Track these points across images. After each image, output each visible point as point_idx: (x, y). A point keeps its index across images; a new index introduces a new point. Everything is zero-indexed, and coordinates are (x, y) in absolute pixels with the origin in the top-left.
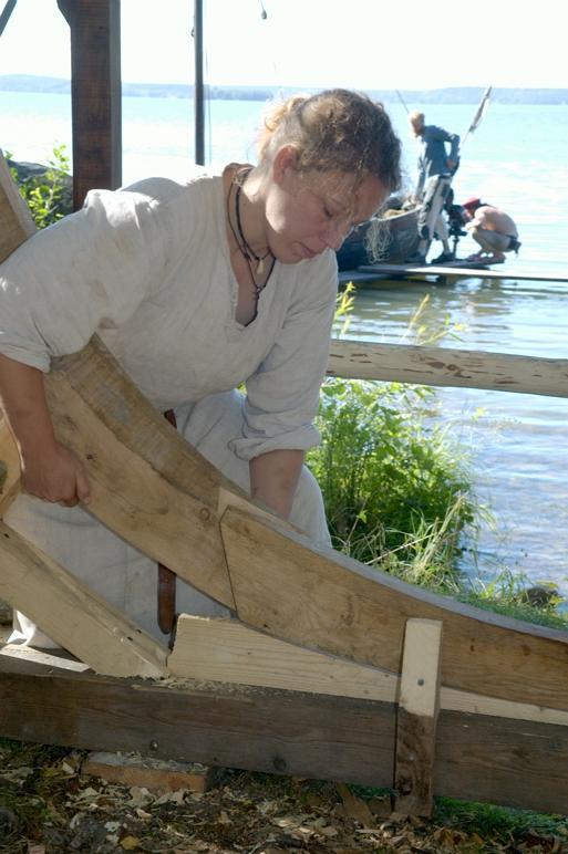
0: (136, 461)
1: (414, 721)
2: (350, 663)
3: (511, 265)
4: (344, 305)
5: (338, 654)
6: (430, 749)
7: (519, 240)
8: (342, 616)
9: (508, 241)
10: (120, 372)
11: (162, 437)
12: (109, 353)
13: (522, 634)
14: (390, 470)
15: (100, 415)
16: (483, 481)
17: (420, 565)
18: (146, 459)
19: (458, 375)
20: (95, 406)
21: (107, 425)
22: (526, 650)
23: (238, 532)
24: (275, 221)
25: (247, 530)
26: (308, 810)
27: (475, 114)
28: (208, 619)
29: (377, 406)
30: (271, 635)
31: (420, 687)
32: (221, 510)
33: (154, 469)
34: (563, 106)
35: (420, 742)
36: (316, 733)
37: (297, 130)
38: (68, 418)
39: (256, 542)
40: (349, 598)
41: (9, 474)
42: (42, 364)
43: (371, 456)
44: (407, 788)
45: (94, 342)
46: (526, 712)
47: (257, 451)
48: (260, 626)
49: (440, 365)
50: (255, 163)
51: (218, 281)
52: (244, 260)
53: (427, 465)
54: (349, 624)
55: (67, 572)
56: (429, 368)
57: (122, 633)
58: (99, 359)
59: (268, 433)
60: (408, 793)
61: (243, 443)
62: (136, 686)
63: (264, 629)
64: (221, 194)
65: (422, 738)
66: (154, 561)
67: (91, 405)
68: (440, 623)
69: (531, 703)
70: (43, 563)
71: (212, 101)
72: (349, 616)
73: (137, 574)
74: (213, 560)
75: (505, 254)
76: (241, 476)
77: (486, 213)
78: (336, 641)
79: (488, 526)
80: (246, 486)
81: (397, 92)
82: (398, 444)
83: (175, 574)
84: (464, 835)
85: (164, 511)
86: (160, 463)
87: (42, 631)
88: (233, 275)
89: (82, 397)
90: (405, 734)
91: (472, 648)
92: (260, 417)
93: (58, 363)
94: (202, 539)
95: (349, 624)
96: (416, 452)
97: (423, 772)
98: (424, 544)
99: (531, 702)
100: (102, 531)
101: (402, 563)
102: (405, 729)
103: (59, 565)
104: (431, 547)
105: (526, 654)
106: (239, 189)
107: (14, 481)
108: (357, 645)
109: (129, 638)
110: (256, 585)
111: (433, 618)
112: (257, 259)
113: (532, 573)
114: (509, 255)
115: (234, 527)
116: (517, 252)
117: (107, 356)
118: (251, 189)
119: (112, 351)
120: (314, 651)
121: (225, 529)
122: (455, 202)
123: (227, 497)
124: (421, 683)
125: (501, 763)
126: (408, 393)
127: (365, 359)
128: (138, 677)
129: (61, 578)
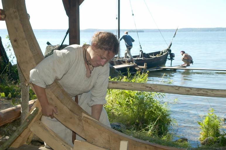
0: (65, 108)
3: (191, 66)
4: (146, 75)
5: (107, 149)
7: (193, 61)
8: (108, 140)
9: (190, 61)
10: (62, 88)
11: (70, 102)
12: (60, 84)
13: (145, 144)
14: (151, 111)
15: (57, 98)
17: (149, 132)
18: (67, 107)
19: (152, 89)
21: (59, 100)
23: (86, 122)
24: (92, 57)
25: (87, 121)
27: (174, 34)
28: (80, 141)
29: (148, 97)
30: (93, 144)
32: (83, 117)
33: (69, 109)
34: (225, 32)
37: (97, 38)
38: (51, 98)
39: (89, 124)
40: (109, 136)
41: (39, 110)
42: (43, 86)
45: (56, 80)
47: (92, 105)
48: (91, 143)
49: (148, 87)
50: (90, 44)
51: (82, 68)
52: (87, 65)
53: (160, 110)
54: (109, 142)
55: (53, 131)
56: (145, 88)
57: (63, 144)
58: (57, 86)
59: (95, 101)
61: (90, 103)
63: (92, 143)
64: (82, 50)
66: (71, 130)
67: (56, 96)
70: (47, 129)
71: (116, 29)
72: (109, 140)
73: (68, 132)
74: (81, 129)
75: (190, 64)
76: (89, 110)
77: (185, 55)
78: (107, 146)
79: (175, 124)
80: (90, 114)
81: (159, 29)
82: (153, 106)
83: (76, 133)
85: (71, 118)
86: (69, 107)
87: (48, 145)
88: (85, 67)
91: (135, 147)
92: (93, 98)
93: (48, 86)
94: (79, 124)
95: (109, 142)
96: (157, 107)
98: (151, 127)
100: (58, 122)
101: (146, 132)
104: (152, 128)
105: (146, 149)
106: (86, 50)
107: (40, 111)
108: (111, 147)
109: (64, 145)
110: (90, 133)
111: (126, 140)
112: (90, 65)
113: (185, 135)
114: (191, 65)
115: (85, 121)
116: (193, 64)
117: (59, 85)
118: (89, 50)
119: (61, 84)
120: (102, 148)
121: (83, 121)
122: (171, 53)
123: (84, 115)
126: (160, 95)
127: (132, 86)
129: (51, 132)
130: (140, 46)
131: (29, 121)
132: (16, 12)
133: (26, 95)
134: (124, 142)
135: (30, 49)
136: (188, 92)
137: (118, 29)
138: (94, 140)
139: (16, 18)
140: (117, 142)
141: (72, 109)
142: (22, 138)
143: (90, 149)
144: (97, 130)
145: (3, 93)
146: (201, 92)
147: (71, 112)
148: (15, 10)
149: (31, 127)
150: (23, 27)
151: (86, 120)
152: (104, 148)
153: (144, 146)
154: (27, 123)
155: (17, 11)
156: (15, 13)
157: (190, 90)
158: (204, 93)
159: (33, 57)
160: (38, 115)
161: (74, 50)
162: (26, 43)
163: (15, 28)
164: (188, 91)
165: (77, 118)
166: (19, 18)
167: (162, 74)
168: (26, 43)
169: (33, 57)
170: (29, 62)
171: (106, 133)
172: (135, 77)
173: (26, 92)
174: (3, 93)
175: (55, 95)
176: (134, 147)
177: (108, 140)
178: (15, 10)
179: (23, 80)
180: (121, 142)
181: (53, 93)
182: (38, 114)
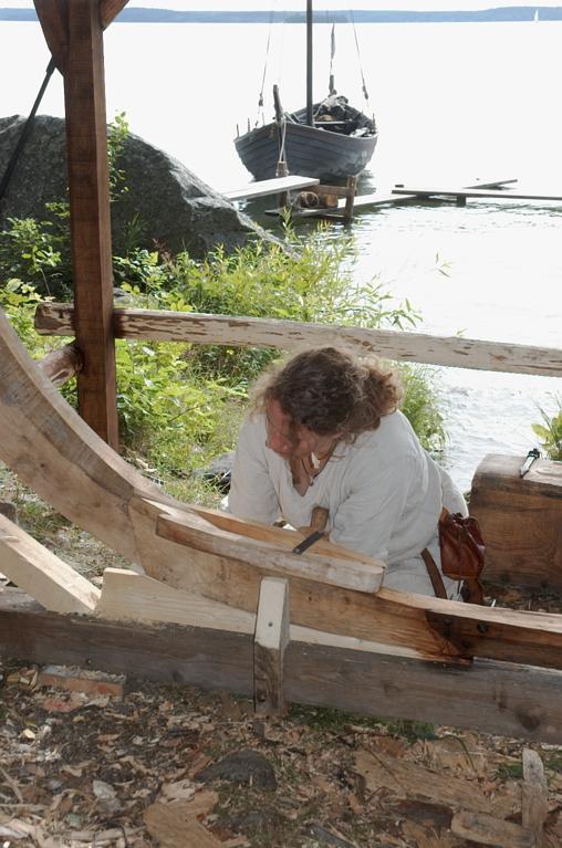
0: (75, 470)
1: (265, 652)
2: (225, 606)
6: (277, 671)
16: (344, 553)
20: (43, 429)
22: (348, 601)
26: (198, 710)
31: (267, 625)
33: (87, 475)
35: (271, 666)
36: (202, 657)
38: (24, 437)
43: (197, 698)
44: (263, 697)
46: (350, 642)
54: (223, 579)
60: (263, 701)
62: (74, 621)
65: (272, 663)
68: (286, 581)
69: (292, 471)
78: (215, 591)
84: (307, 729)
85: (98, 505)
89: (33, 423)
90: (259, 660)
95: (223, 579)
97: (273, 686)
99: (353, 636)
102: (260, 657)
103: (246, 324)
124: (271, 625)
125: (330, 680)
128: (76, 614)
130: (364, 89)
136: (498, 361)
137: (305, 9)
138: (171, 570)
140: (248, 579)
141: (99, 476)
145: (340, 201)
146: (545, 362)
147: (95, 484)
153: (342, 596)
157: (506, 354)
158: (552, 365)
164: (500, 358)
165: (118, 505)
174: (340, 201)
175: (36, 426)
176: (385, 565)
177: (221, 573)
180: (263, 582)
181: (30, 419)
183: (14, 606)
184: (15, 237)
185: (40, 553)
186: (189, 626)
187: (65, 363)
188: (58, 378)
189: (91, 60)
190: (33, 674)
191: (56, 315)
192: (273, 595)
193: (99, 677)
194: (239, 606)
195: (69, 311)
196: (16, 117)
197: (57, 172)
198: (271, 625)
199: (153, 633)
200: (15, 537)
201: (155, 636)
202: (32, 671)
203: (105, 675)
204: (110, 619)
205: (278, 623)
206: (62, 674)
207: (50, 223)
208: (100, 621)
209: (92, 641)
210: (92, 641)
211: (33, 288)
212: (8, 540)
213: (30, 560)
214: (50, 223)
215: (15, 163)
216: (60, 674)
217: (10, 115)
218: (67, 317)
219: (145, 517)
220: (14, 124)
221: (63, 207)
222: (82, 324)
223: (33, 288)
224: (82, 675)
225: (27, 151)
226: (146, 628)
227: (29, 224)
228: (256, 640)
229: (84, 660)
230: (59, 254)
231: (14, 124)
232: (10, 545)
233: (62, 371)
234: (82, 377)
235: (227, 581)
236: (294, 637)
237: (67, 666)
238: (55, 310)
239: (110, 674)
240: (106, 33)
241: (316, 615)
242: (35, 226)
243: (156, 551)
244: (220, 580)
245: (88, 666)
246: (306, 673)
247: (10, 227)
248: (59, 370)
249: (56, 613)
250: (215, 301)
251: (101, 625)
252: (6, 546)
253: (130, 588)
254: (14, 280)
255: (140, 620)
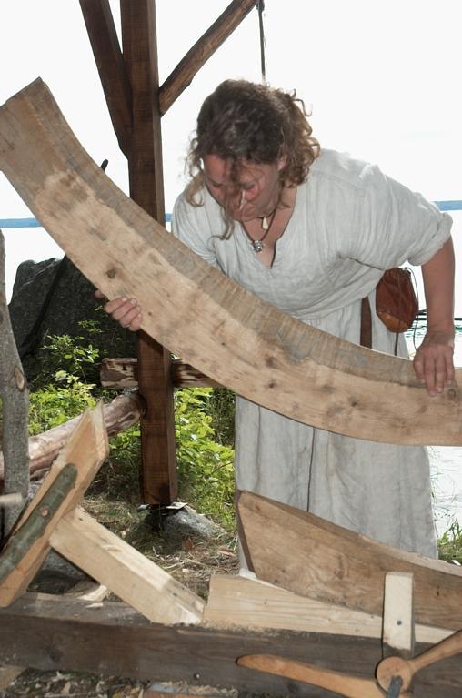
2: (344, 608)
23: (251, 510)
25: (258, 508)
39: (266, 517)
40: (340, 558)
54: (341, 577)
62: (180, 632)
68: (411, 575)
72: (341, 572)
91: (438, 594)
111: (407, 571)
120: (314, 599)
124: (399, 623)
128: (182, 624)
131: (49, 514)
132: (72, 179)
133: (19, 423)
134: (397, 577)
135: (176, 268)
138: (284, 571)
139: (81, 196)
140: (369, 575)
142: (20, 573)
143: (269, 603)
144: (295, 536)
148: (63, 175)
149: (54, 535)
150: (119, 212)
151: (251, 503)
152: (320, 598)
154: (43, 520)
155: (75, 172)
156: (68, 185)
159: (201, 291)
160: (77, 492)
161: (93, 226)
162: (154, 259)
163: (92, 231)
166: (90, 192)
167: (435, 205)
168: (154, 259)
169: (199, 288)
170: (193, 314)
171: (330, 546)
172: (124, 272)
173: (18, 410)
178: (63, 175)
179: (8, 370)
180: (387, 577)
182: (77, 487)
183: (117, 620)
184: (53, 350)
185: (142, 562)
186: (303, 632)
187: (132, 407)
188: (126, 420)
189: (152, 139)
190: (139, 693)
191: (119, 369)
192: (399, 590)
193: (209, 692)
194: (359, 607)
195: (132, 364)
196: (54, 259)
197: (86, 299)
198: (399, 623)
199: (267, 640)
200: (116, 547)
201: (269, 644)
202: (137, 689)
203: (215, 690)
204: (219, 628)
205: (407, 620)
206: (170, 690)
207: (82, 338)
208: (208, 630)
209: (200, 652)
210: (200, 652)
211: (77, 378)
212: (110, 549)
213: (133, 569)
214: (82, 338)
215: (52, 294)
216: (167, 691)
217: (48, 258)
218: (129, 369)
219: (257, 515)
220: (52, 265)
221: (93, 324)
222: (145, 374)
223: (77, 378)
224: (191, 691)
225: (62, 284)
226: (258, 635)
227: (66, 339)
228: (384, 641)
229: (191, 674)
230: (97, 351)
231: (52, 265)
232: (113, 554)
233: (130, 414)
234: (145, 422)
235: (345, 579)
236: (419, 639)
237: (173, 682)
238: (119, 364)
239: (220, 688)
240: (163, 119)
241: (445, 612)
242: (70, 340)
243: (268, 551)
244: (337, 579)
245: (194, 680)
246: (437, 677)
247: (50, 342)
248: (127, 413)
249: (161, 625)
250: (222, 392)
251: (210, 635)
252: (109, 555)
253: (239, 594)
254: (61, 372)
255: (251, 628)
